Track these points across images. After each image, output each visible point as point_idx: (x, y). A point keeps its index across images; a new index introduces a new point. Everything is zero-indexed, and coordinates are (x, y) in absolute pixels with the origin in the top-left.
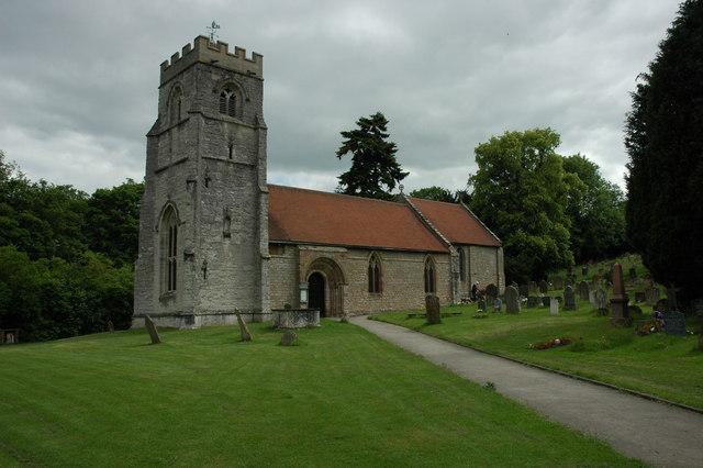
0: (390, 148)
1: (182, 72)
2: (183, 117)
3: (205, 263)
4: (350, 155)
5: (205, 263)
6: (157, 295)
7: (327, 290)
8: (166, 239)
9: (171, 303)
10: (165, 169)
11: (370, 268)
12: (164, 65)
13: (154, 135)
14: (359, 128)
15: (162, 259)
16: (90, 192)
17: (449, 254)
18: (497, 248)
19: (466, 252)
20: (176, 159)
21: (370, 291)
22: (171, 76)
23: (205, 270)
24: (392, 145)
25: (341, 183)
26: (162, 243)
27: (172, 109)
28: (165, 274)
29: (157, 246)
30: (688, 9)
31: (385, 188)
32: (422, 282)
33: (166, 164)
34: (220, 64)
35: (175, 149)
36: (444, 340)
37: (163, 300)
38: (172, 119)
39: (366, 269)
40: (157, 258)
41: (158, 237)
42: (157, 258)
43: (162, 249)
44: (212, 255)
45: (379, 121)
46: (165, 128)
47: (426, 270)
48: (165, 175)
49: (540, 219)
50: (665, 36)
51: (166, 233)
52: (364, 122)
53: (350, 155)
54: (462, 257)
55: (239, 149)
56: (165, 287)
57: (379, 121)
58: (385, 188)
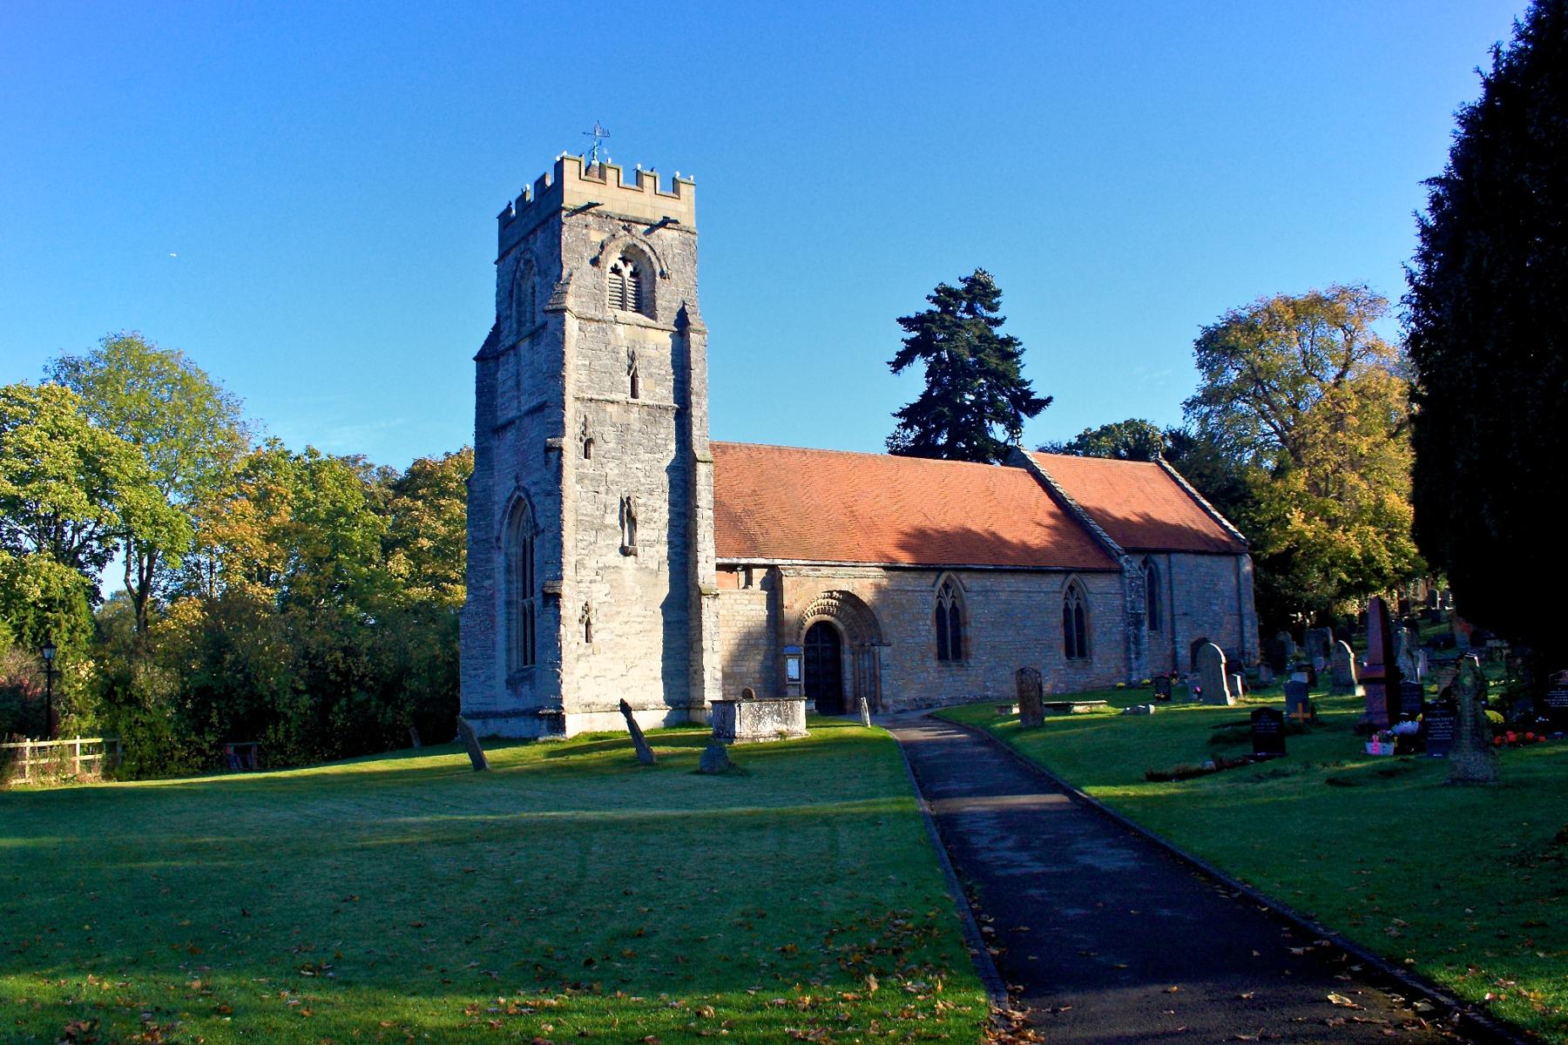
0: (1007, 350)
1: (534, 231)
2: (539, 320)
3: (587, 608)
4: (920, 366)
5: (587, 608)
6: (501, 676)
7: (847, 658)
8: (516, 562)
9: (526, 689)
10: (511, 423)
11: (940, 611)
12: (504, 218)
13: (488, 358)
14: (936, 308)
15: (509, 603)
16: (1024, 375)
17: (1120, 571)
18: (1237, 555)
19: (1162, 567)
20: (528, 403)
21: (942, 656)
22: (516, 239)
23: (588, 624)
24: (1009, 341)
25: (905, 426)
26: (508, 570)
27: (520, 304)
28: (517, 628)
29: (500, 577)
30: (1543, 31)
31: (999, 432)
32: (1059, 635)
33: (512, 414)
34: (606, 208)
35: (526, 383)
36: (764, 756)
37: (512, 683)
38: (520, 323)
39: (931, 612)
40: (500, 599)
41: (499, 560)
42: (500, 599)
43: (509, 582)
44: (599, 594)
45: (980, 291)
46: (508, 343)
47: (1067, 611)
48: (510, 435)
49: (489, 561)
50: (1475, 94)
51: (516, 550)
52: (945, 297)
53: (920, 366)
54: (1153, 579)
55: (651, 375)
56: (516, 657)
57: (980, 291)
58: (999, 432)
